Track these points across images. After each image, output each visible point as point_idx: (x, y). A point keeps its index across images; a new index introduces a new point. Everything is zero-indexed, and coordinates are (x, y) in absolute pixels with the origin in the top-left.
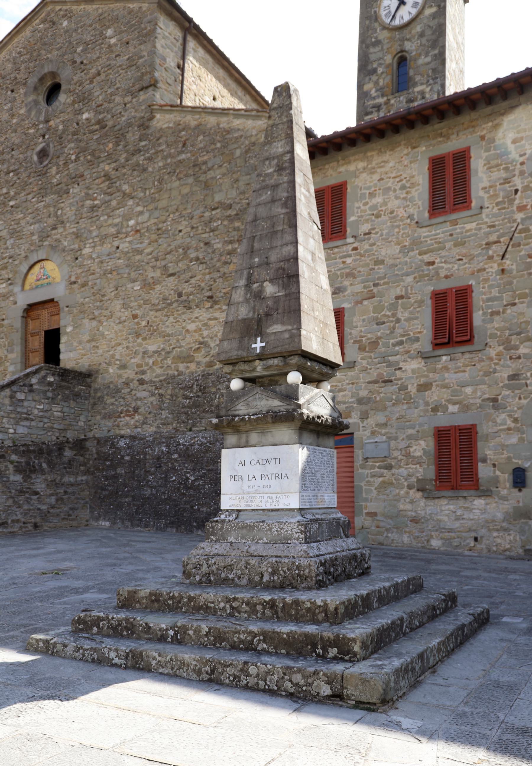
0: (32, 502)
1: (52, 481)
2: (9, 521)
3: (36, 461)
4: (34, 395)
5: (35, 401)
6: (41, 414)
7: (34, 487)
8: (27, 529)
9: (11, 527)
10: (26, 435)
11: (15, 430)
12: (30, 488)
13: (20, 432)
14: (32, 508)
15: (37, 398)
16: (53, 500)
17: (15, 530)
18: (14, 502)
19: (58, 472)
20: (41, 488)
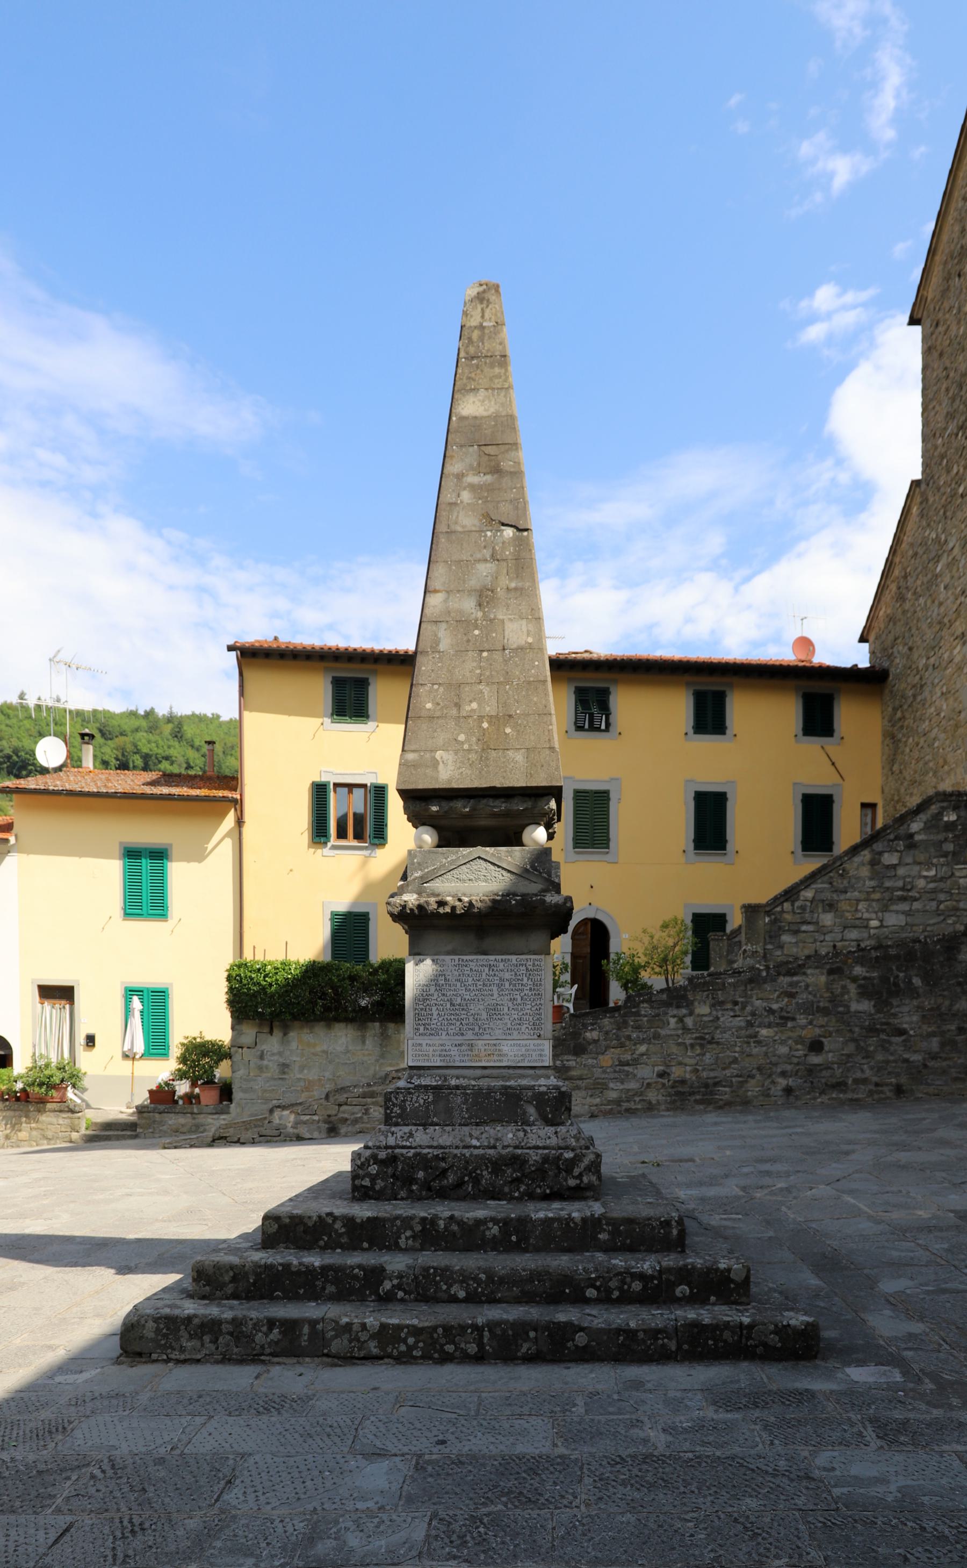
0: (892, 1048)
1: (931, 1009)
2: (850, 1081)
3: (901, 975)
4: (917, 852)
5: (920, 863)
6: (932, 885)
7: (896, 1021)
8: (883, 1096)
9: (853, 1091)
10: (902, 928)
11: (881, 921)
12: (887, 1024)
13: (890, 924)
14: (891, 1058)
15: (922, 857)
16: (935, 1043)
17: (860, 1096)
18: (858, 1048)
19: (946, 993)
20: (912, 1022)
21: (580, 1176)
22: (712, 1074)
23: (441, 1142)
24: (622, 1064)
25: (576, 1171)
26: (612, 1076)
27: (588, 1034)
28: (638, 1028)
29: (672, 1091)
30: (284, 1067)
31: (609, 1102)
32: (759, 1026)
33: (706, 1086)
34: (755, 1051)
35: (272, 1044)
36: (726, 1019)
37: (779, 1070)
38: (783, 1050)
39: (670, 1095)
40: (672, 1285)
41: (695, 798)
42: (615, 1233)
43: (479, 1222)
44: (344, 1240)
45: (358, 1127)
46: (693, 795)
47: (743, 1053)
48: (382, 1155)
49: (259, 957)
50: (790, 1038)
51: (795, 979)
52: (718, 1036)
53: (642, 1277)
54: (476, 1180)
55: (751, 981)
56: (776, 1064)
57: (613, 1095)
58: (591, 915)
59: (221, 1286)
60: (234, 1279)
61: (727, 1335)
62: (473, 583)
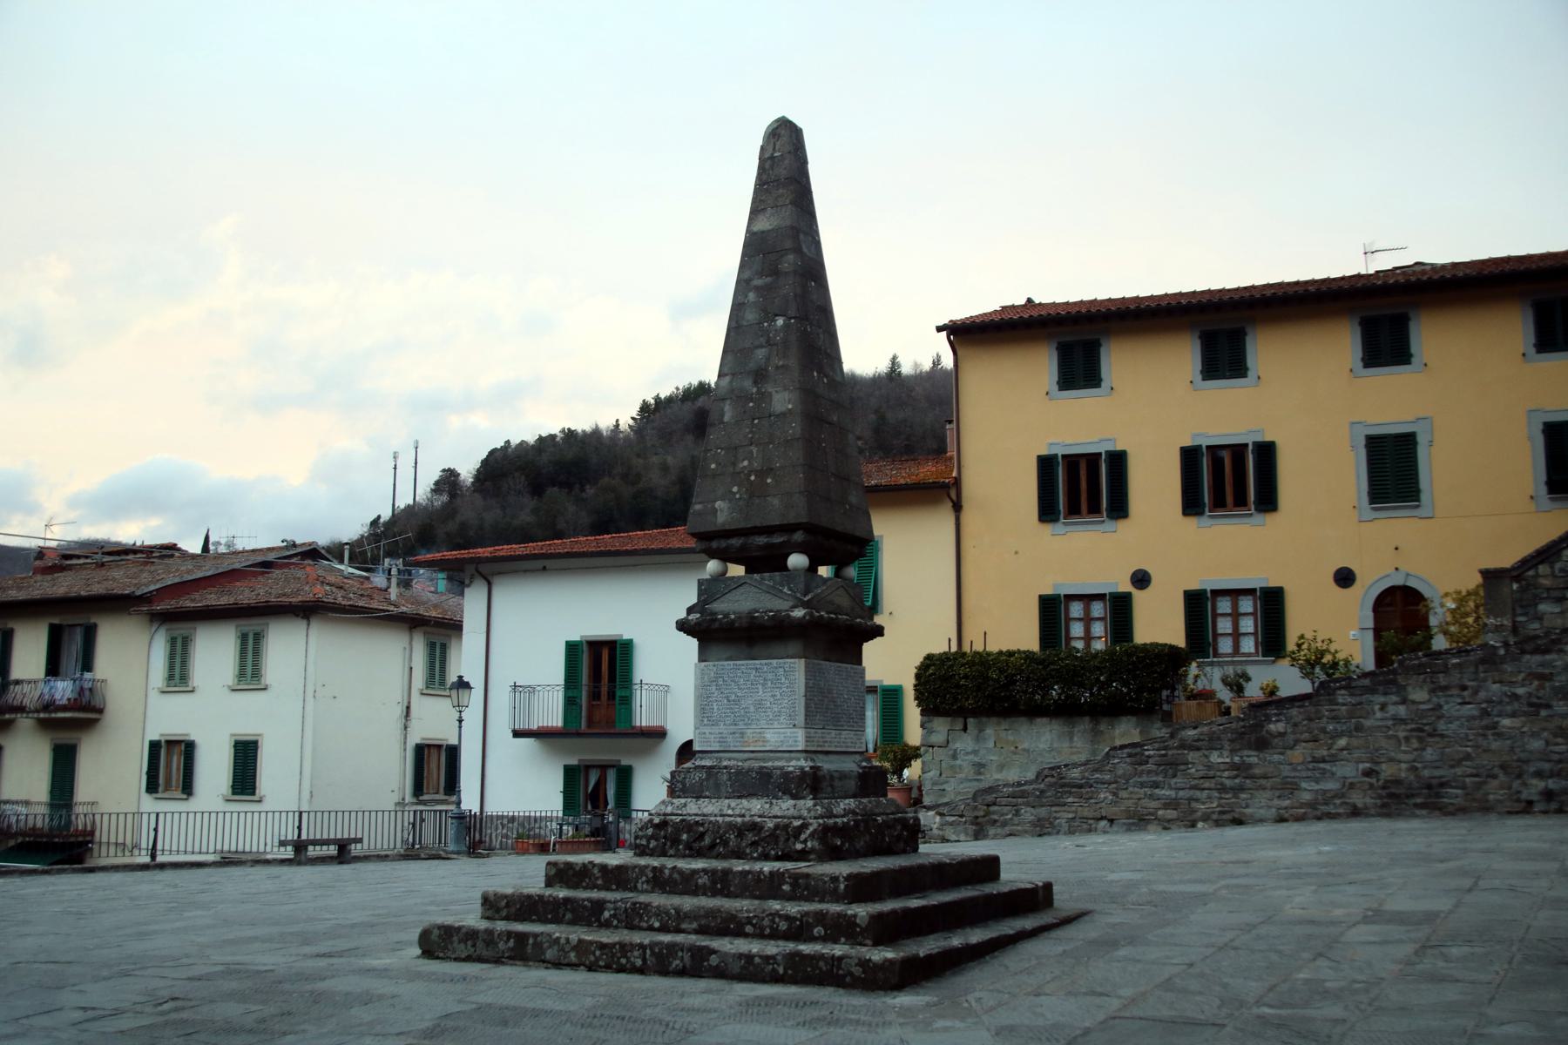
21: (805, 841)
22: (1437, 773)
23: (705, 811)
24: (1315, 760)
25: (803, 837)
26: (1304, 774)
27: (1272, 727)
28: (1335, 719)
29: (1384, 793)
30: (980, 767)
31: (1302, 805)
32: (1499, 716)
33: (1429, 787)
34: (1495, 745)
35: (964, 743)
36: (1451, 707)
37: (1532, 769)
38: (1537, 744)
39: (1380, 797)
40: (811, 927)
41: (1543, 431)
42: (795, 885)
43: (695, 872)
44: (600, 882)
45: (1007, 829)
46: (1541, 427)
47: (1478, 747)
48: (657, 820)
49: (979, 647)
50: (1544, 729)
51: (1548, 657)
52: (1441, 726)
53: (787, 918)
54: (725, 843)
55: (1483, 661)
56: (1527, 762)
57: (1307, 797)
58: (1398, 581)
59: (498, 910)
60: (507, 906)
61: (821, 964)
62: (752, 365)
